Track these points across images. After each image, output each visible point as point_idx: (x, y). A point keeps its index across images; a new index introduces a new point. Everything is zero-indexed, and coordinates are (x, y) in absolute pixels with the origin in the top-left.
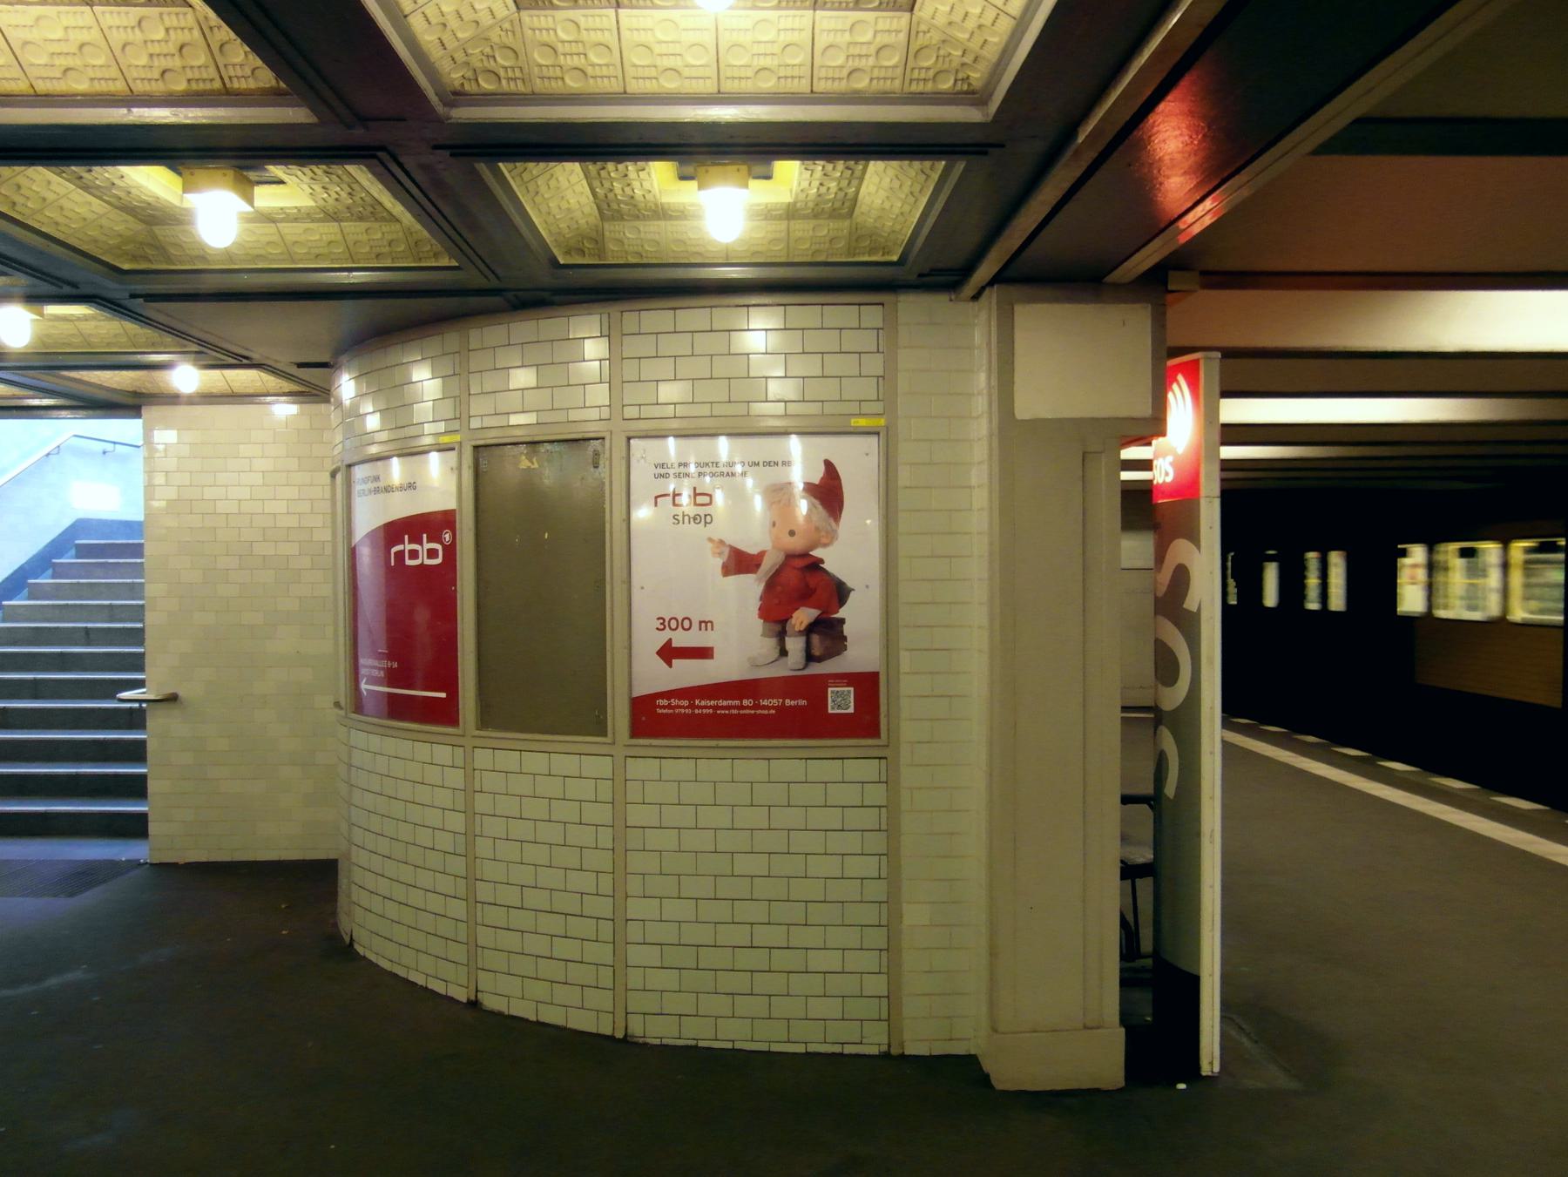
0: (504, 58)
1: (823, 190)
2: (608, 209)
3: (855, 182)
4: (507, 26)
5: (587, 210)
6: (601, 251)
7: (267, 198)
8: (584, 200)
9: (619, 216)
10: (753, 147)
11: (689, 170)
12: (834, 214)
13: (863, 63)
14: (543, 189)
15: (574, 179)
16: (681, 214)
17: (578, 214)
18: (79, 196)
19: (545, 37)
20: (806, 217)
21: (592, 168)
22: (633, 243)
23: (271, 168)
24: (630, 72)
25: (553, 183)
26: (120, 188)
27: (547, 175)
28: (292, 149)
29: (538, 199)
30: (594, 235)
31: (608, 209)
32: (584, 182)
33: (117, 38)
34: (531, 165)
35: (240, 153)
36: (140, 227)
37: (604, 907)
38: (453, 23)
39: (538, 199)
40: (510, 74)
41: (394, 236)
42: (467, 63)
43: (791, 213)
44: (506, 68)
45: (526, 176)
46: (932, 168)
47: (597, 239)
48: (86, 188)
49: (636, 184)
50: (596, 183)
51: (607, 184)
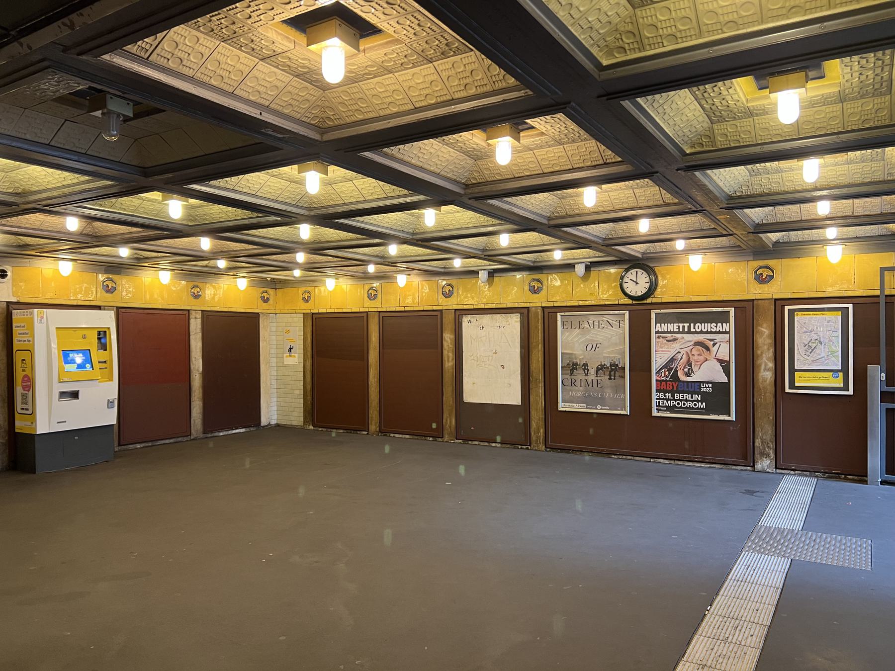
0: (628, 38)
1: (863, 78)
2: (714, 116)
3: (887, 69)
4: (628, 20)
5: (701, 119)
6: (714, 142)
7: (527, 138)
8: (697, 113)
9: (722, 119)
10: (772, 62)
11: (763, 82)
12: (877, 93)
13: (467, 81)
14: (668, 111)
15: (688, 101)
16: (764, 112)
17: (695, 123)
18: (446, 149)
19: (650, 21)
20: (854, 99)
21: (698, 91)
22: (729, 134)
23: (528, 121)
24: (414, 100)
25: (674, 106)
26: (460, 142)
27: (670, 102)
28: (544, 107)
29: (666, 117)
30: (708, 133)
31: (714, 116)
32: (695, 102)
33: (444, 75)
34: (657, 96)
35: (510, 116)
36: (470, 161)
37: (756, 621)
38: (597, 26)
39: (666, 117)
40: (632, 46)
41: (592, 149)
42: (607, 46)
43: (842, 98)
44: (648, 38)
45: (656, 105)
46: (884, 54)
47: (711, 136)
48: (447, 144)
49: (728, 98)
50: (703, 102)
51: (710, 101)
